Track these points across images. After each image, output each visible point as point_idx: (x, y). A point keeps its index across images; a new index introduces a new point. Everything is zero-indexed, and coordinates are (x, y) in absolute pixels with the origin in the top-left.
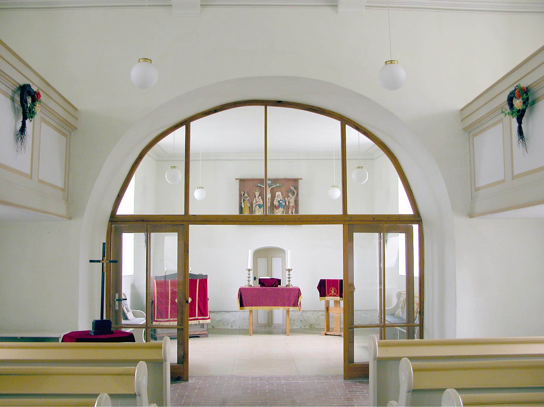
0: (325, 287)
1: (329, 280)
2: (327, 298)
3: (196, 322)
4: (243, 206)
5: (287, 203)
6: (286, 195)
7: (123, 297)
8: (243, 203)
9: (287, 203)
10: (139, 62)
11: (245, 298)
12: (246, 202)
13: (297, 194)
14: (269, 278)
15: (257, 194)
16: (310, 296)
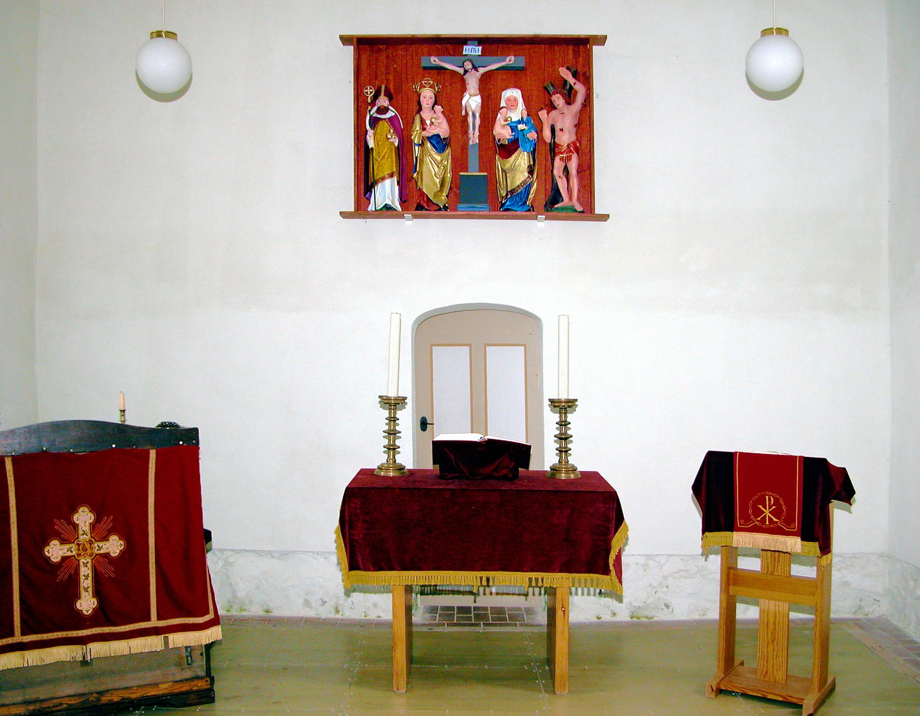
0: (727, 489)
1: (742, 455)
2: (740, 539)
3: (154, 643)
4: (371, 144)
5: (547, 134)
6: (539, 102)
7: (804, 661)
8: (370, 132)
9: (547, 134)
10: (152, 38)
11: (383, 522)
12: (384, 127)
13: (588, 103)
14: (476, 437)
15: (427, 95)
16: (661, 527)
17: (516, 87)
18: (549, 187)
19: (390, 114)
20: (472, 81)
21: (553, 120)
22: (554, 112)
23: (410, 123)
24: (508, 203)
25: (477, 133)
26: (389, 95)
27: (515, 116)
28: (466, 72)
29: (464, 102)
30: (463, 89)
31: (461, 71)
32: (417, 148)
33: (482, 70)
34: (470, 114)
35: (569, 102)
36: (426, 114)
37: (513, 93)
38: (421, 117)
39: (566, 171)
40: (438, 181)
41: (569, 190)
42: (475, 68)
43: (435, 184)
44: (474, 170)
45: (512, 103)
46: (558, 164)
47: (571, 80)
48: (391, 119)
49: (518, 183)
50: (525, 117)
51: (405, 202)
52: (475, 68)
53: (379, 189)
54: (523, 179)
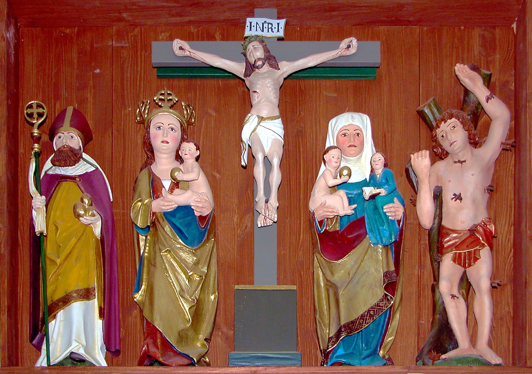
4: (40, 224)
12: (66, 193)
15: (165, 126)
17: (358, 109)
18: (426, 320)
19: (85, 166)
20: (265, 90)
21: (439, 179)
22: (441, 165)
23: (127, 190)
24: (341, 351)
25: (274, 202)
26: (81, 125)
27: (360, 171)
28: (251, 68)
29: (246, 134)
30: (246, 104)
31: (237, 68)
32: (142, 238)
33: (287, 68)
34: (260, 157)
35: (475, 142)
36: (163, 166)
37: (351, 123)
38: (151, 174)
39: (466, 286)
40: (187, 307)
41: (472, 323)
42: (271, 59)
43: (181, 311)
44: (266, 277)
45: (351, 142)
46: (448, 267)
47: (480, 91)
48: (86, 178)
49: (362, 310)
50: (379, 170)
51: (117, 353)
52: (271, 59)
53: (55, 327)
54: (373, 301)
